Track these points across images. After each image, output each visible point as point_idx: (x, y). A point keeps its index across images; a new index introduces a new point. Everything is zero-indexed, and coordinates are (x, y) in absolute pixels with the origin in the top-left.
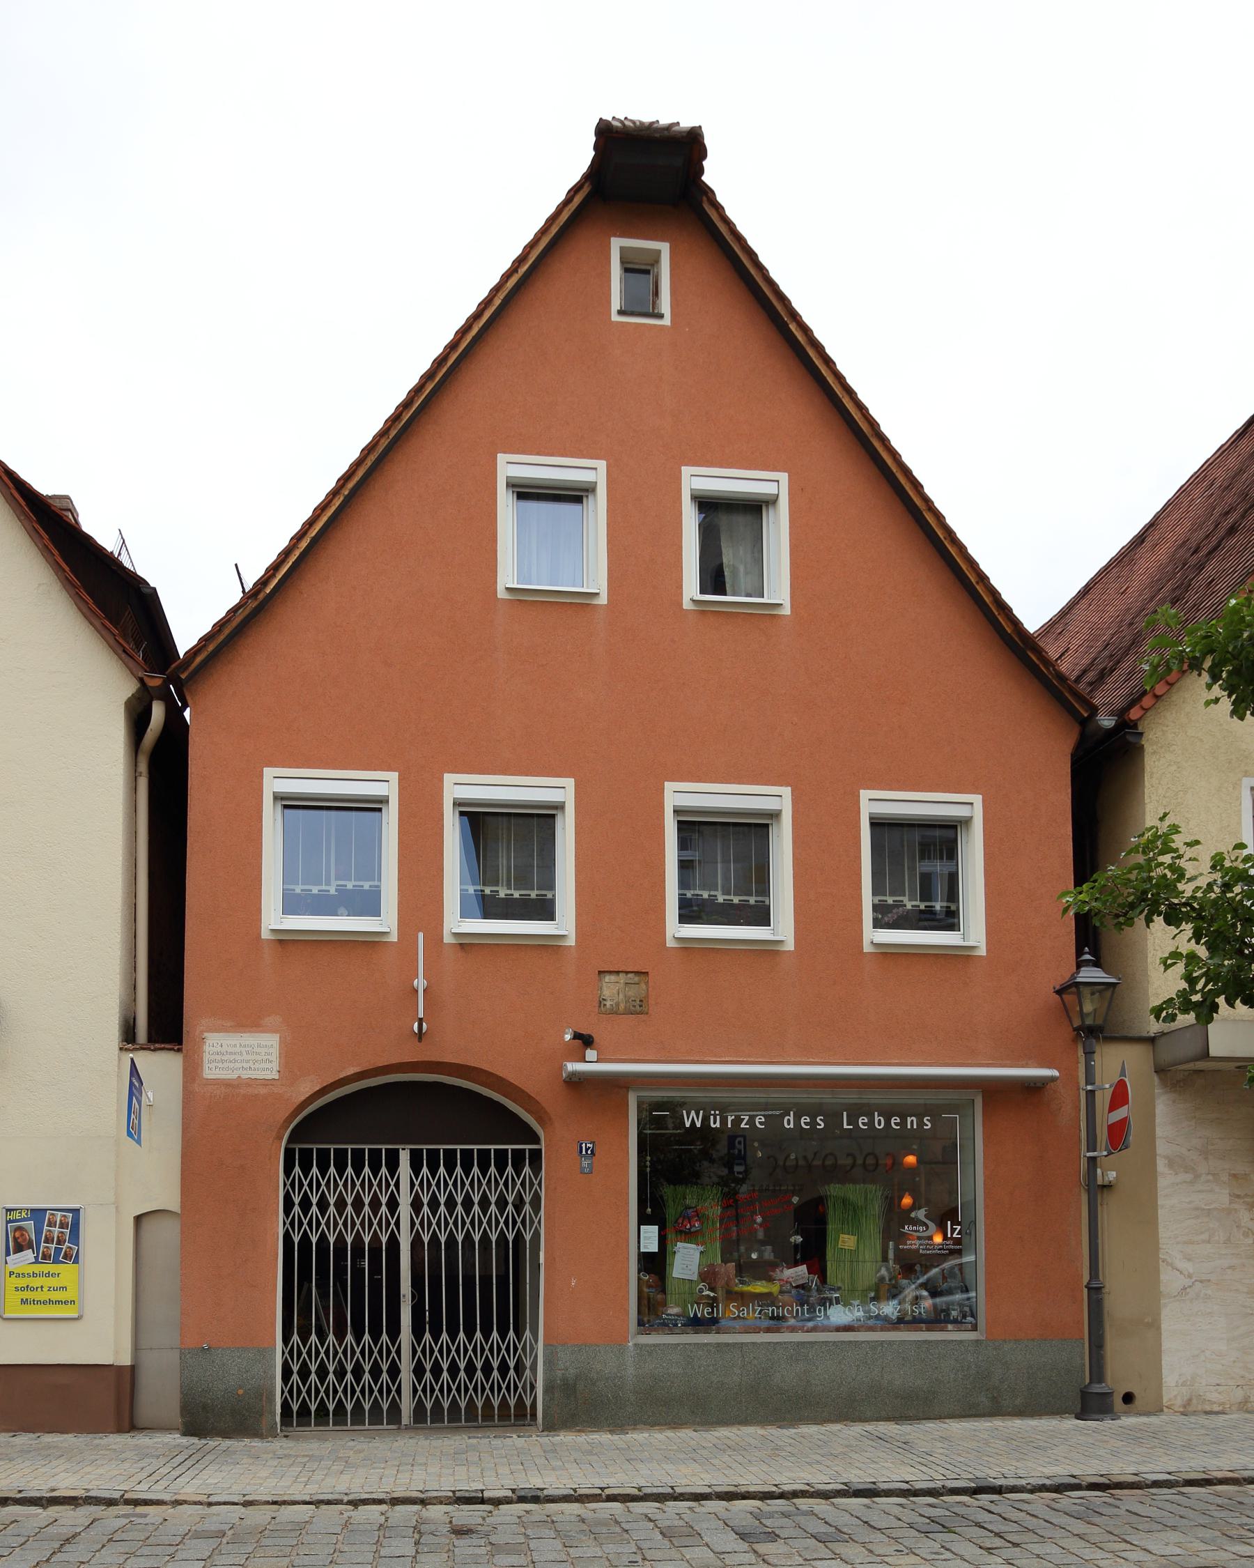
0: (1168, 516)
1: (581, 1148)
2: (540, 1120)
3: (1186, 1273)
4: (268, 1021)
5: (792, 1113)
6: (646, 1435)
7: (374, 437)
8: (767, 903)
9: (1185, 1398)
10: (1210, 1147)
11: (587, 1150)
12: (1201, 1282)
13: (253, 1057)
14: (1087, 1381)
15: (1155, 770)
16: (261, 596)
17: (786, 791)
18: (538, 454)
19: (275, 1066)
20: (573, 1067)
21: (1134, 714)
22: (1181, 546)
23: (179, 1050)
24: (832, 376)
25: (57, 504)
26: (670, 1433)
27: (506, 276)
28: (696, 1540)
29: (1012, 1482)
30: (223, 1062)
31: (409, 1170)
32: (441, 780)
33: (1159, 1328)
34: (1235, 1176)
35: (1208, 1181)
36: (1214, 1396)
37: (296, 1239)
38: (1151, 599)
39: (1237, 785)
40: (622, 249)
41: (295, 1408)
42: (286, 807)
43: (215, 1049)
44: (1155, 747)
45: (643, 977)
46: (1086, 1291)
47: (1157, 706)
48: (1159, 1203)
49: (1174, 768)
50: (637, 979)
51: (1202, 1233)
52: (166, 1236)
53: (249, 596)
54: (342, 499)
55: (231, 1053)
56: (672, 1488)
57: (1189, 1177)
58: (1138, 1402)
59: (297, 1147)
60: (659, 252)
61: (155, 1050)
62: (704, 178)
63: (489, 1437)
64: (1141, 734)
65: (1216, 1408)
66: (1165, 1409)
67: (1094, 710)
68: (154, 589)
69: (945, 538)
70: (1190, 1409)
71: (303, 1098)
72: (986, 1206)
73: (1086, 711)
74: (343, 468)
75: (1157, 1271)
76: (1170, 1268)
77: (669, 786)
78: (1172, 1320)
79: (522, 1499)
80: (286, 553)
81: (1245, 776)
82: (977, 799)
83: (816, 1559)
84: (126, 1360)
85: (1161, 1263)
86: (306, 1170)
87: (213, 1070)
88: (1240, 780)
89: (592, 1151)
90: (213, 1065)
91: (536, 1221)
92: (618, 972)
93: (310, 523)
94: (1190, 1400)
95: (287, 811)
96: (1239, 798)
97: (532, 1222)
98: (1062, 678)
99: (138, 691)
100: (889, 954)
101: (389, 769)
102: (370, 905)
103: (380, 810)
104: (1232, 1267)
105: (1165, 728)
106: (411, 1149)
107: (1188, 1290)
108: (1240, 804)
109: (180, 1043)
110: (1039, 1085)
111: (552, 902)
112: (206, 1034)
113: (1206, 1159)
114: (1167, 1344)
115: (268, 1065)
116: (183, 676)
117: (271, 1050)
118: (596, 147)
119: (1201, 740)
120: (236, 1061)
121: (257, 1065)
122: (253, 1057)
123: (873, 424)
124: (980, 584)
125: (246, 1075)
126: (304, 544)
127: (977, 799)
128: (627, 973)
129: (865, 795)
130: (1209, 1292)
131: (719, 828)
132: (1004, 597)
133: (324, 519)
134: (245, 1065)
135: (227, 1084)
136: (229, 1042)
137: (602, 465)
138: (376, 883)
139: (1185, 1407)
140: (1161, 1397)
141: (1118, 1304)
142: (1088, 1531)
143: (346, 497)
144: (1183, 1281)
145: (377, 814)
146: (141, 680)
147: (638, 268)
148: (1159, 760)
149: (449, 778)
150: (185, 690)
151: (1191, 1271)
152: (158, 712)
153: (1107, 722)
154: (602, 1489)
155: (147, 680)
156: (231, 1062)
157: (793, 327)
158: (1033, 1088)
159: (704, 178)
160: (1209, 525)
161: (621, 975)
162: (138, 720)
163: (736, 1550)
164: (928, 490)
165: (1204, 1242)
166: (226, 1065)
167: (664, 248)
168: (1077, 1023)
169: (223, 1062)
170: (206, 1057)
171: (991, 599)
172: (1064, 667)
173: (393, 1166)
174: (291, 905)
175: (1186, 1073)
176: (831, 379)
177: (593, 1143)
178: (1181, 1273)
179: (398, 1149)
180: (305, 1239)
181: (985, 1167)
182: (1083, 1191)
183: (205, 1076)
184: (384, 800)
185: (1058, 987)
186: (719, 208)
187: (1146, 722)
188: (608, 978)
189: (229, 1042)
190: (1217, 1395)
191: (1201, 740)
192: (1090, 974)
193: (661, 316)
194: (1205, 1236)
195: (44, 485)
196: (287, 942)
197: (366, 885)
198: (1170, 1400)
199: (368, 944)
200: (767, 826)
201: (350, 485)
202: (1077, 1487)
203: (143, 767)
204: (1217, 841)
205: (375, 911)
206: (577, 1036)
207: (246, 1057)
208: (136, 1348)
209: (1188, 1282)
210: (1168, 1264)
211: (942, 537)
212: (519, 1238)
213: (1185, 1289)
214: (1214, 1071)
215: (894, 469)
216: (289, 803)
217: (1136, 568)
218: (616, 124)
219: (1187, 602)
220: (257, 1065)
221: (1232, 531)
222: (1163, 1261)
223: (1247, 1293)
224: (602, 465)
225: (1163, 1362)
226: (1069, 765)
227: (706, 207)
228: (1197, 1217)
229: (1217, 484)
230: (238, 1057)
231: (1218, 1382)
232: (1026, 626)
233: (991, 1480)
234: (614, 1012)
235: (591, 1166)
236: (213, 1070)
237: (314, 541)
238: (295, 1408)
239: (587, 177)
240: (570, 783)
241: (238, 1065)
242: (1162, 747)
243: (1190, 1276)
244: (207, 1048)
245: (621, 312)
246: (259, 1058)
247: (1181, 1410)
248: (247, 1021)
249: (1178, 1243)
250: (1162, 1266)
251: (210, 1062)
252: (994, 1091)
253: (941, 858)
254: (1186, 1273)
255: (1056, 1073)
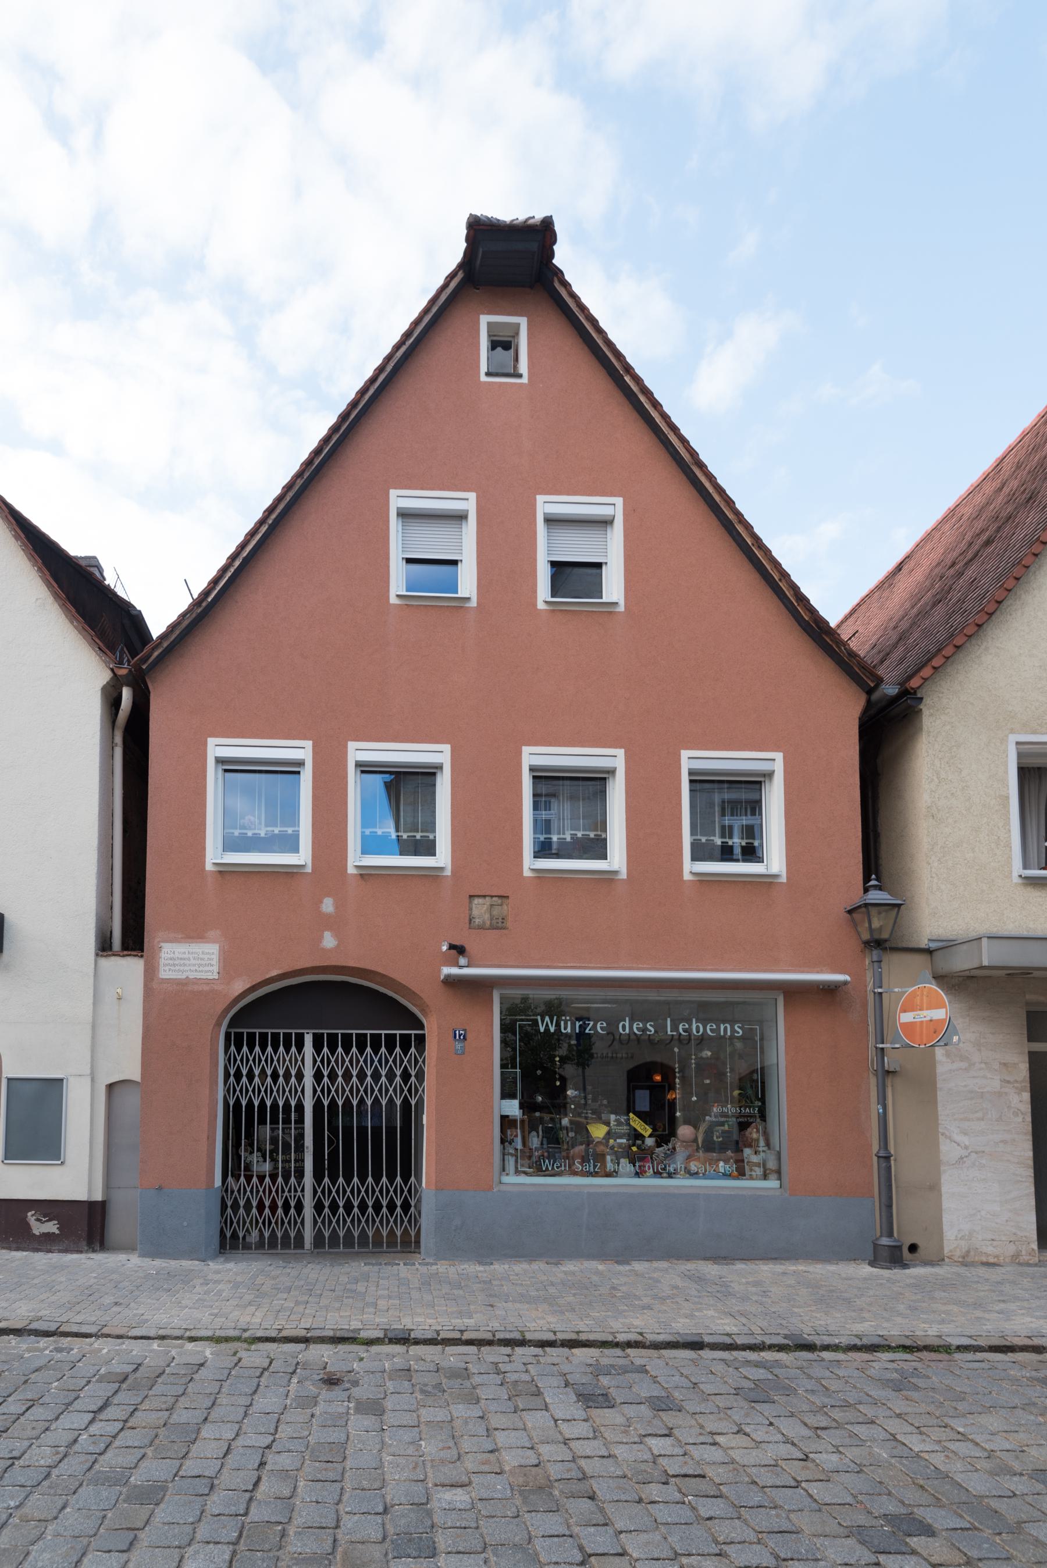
0: (922, 548)
1: (455, 1034)
2: (423, 1011)
3: (963, 1145)
4: (212, 934)
5: (627, 1019)
6: (506, 1266)
7: (292, 478)
8: (604, 836)
9: (964, 1251)
10: (982, 1041)
11: (460, 1036)
12: (976, 1153)
13: (199, 962)
14: (878, 1234)
15: (931, 730)
16: (204, 604)
17: (620, 753)
18: (422, 489)
19: (216, 969)
20: (447, 970)
21: (914, 683)
22: (939, 564)
23: (142, 956)
24: (660, 417)
25: (83, 563)
26: (525, 1266)
27: (397, 347)
28: (537, 1402)
29: (827, 1340)
30: (174, 965)
31: (312, 1049)
32: (346, 747)
33: (940, 1191)
34: (1005, 1064)
35: (981, 1069)
36: (990, 1250)
37: (231, 1103)
38: (913, 607)
39: (1004, 740)
40: (489, 324)
41: (228, 1235)
42: (226, 771)
43: (169, 956)
44: (931, 711)
45: (504, 900)
46: (875, 1159)
47: (934, 676)
48: (938, 1086)
49: (948, 727)
50: (500, 901)
51: (976, 1112)
52: (131, 1103)
53: (197, 603)
54: (267, 527)
55: (181, 959)
56: (522, 1332)
57: (964, 1065)
58: (921, 1252)
59: (233, 1031)
60: (518, 325)
61: (124, 956)
62: (554, 261)
63: (381, 1264)
64: (921, 699)
65: (992, 1260)
66: (947, 1260)
67: (879, 681)
68: (140, 611)
69: (753, 545)
70: (969, 1259)
71: (237, 994)
72: (788, 1086)
73: (872, 681)
74: (268, 502)
75: (936, 1145)
76: (948, 1141)
77: (526, 750)
78: (950, 1184)
79: (392, 1341)
80: (224, 570)
81: (1011, 733)
82: (779, 756)
83: (650, 1435)
84: (98, 1197)
85: (940, 1136)
86: (239, 1049)
87: (165, 973)
88: (1007, 736)
89: (464, 1037)
90: (167, 968)
91: (421, 1090)
92: (484, 896)
93: (242, 546)
94: (968, 1252)
95: (228, 775)
96: (1006, 751)
97: (417, 1091)
98: (852, 654)
99: (112, 679)
100: (705, 881)
101: (305, 738)
102: (291, 844)
103: (299, 773)
104: (1005, 1142)
105: (941, 695)
106: (314, 1034)
107: (965, 1159)
108: (1007, 756)
109: (142, 950)
110: (832, 987)
111: (434, 842)
112: (162, 944)
113: (979, 1050)
114: (947, 1203)
115: (211, 968)
116: (144, 667)
117: (213, 956)
118: (468, 239)
119: (972, 704)
120: (185, 965)
121: (201, 968)
122: (199, 962)
123: (693, 454)
124: (783, 581)
125: (192, 975)
126: (237, 563)
127: (779, 756)
128: (492, 897)
129: (685, 754)
130: (984, 1162)
131: (568, 782)
132: (803, 590)
133: (253, 543)
134: (193, 968)
135: (183, 983)
136: (179, 950)
137: (472, 496)
138: (296, 829)
139: (964, 1257)
140: (942, 1248)
141: (905, 1170)
142: (909, 1410)
143: (270, 526)
144: (959, 1152)
145: (296, 776)
146: (112, 670)
147: (502, 343)
148: (935, 721)
149: (352, 745)
150: (148, 680)
151: (967, 1143)
152: (126, 694)
153: (890, 690)
154: (462, 1332)
155: (115, 670)
156: (181, 965)
157: (627, 379)
158: (829, 991)
159: (554, 261)
160: (963, 545)
161: (487, 898)
162: (112, 702)
163: (576, 1417)
164: (739, 506)
165: (978, 1119)
166: (177, 968)
167: (523, 322)
168: (866, 936)
169: (174, 965)
170: (162, 962)
171: (792, 592)
172: (853, 645)
173: (300, 1046)
174: (231, 845)
175: (961, 979)
176: (658, 420)
177: (465, 1030)
178: (958, 1145)
179: (303, 1034)
180: (238, 1103)
181: (787, 1053)
182: (871, 1075)
183: (161, 977)
184: (301, 763)
185: (849, 908)
186: (566, 285)
187: (924, 691)
188: (476, 901)
189: (179, 950)
190: (992, 1249)
191: (972, 704)
192: (876, 896)
193: (520, 376)
194: (979, 1115)
195: (74, 546)
196: (226, 872)
197: (290, 830)
198: (951, 1251)
199: (290, 873)
200: (605, 779)
201: (273, 516)
202: (889, 1348)
203: (119, 739)
204: (986, 787)
205: (295, 849)
206: (452, 947)
207: (193, 962)
208: (107, 1186)
209: (964, 1153)
210: (946, 1137)
211: (750, 544)
212: (406, 1103)
213: (962, 1158)
214: (986, 977)
215: (711, 490)
216: (229, 766)
217: (895, 589)
218: (482, 218)
219: (950, 600)
220: (201, 968)
221: (988, 543)
222: (942, 1135)
223: (1018, 1163)
224: (472, 496)
225: (944, 1219)
226: (857, 727)
227: (557, 285)
228: (972, 1099)
229: (965, 518)
230: (187, 962)
231: (994, 1238)
232: (823, 613)
233: (806, 1336)
234: (481, 927)
235: (463, 1048)
236: (165, 973)
237: (246, 561)
238: (228, 1235)
239: (460, 266)
240: (447, 748)
241: (186, 968)
242: (938, 710)
243: (966, 1148)
244: (163, 955)
245: (488, 374)
246: (203, 962)
247: (960, 1260)
248: (194, 934)
249: (955, 1120)
250: (941, 1139)
251: (165, 965)
252: (793, 992)
253: (746, 815)
254: (963, 1145)
255: (847, 978)
